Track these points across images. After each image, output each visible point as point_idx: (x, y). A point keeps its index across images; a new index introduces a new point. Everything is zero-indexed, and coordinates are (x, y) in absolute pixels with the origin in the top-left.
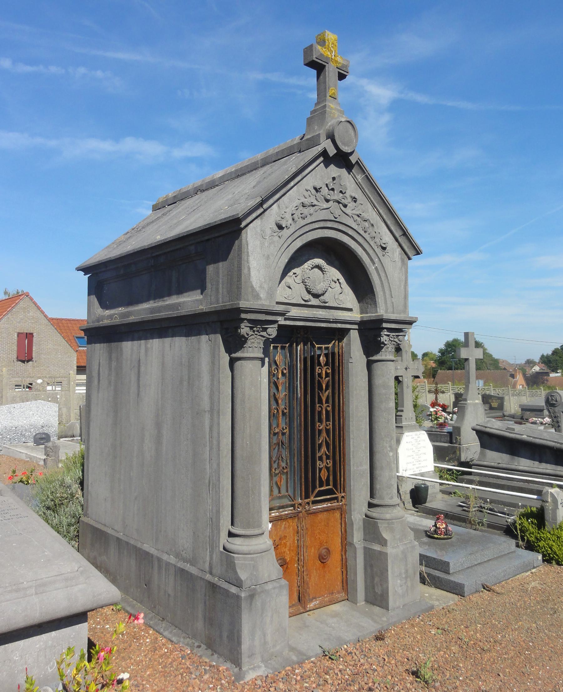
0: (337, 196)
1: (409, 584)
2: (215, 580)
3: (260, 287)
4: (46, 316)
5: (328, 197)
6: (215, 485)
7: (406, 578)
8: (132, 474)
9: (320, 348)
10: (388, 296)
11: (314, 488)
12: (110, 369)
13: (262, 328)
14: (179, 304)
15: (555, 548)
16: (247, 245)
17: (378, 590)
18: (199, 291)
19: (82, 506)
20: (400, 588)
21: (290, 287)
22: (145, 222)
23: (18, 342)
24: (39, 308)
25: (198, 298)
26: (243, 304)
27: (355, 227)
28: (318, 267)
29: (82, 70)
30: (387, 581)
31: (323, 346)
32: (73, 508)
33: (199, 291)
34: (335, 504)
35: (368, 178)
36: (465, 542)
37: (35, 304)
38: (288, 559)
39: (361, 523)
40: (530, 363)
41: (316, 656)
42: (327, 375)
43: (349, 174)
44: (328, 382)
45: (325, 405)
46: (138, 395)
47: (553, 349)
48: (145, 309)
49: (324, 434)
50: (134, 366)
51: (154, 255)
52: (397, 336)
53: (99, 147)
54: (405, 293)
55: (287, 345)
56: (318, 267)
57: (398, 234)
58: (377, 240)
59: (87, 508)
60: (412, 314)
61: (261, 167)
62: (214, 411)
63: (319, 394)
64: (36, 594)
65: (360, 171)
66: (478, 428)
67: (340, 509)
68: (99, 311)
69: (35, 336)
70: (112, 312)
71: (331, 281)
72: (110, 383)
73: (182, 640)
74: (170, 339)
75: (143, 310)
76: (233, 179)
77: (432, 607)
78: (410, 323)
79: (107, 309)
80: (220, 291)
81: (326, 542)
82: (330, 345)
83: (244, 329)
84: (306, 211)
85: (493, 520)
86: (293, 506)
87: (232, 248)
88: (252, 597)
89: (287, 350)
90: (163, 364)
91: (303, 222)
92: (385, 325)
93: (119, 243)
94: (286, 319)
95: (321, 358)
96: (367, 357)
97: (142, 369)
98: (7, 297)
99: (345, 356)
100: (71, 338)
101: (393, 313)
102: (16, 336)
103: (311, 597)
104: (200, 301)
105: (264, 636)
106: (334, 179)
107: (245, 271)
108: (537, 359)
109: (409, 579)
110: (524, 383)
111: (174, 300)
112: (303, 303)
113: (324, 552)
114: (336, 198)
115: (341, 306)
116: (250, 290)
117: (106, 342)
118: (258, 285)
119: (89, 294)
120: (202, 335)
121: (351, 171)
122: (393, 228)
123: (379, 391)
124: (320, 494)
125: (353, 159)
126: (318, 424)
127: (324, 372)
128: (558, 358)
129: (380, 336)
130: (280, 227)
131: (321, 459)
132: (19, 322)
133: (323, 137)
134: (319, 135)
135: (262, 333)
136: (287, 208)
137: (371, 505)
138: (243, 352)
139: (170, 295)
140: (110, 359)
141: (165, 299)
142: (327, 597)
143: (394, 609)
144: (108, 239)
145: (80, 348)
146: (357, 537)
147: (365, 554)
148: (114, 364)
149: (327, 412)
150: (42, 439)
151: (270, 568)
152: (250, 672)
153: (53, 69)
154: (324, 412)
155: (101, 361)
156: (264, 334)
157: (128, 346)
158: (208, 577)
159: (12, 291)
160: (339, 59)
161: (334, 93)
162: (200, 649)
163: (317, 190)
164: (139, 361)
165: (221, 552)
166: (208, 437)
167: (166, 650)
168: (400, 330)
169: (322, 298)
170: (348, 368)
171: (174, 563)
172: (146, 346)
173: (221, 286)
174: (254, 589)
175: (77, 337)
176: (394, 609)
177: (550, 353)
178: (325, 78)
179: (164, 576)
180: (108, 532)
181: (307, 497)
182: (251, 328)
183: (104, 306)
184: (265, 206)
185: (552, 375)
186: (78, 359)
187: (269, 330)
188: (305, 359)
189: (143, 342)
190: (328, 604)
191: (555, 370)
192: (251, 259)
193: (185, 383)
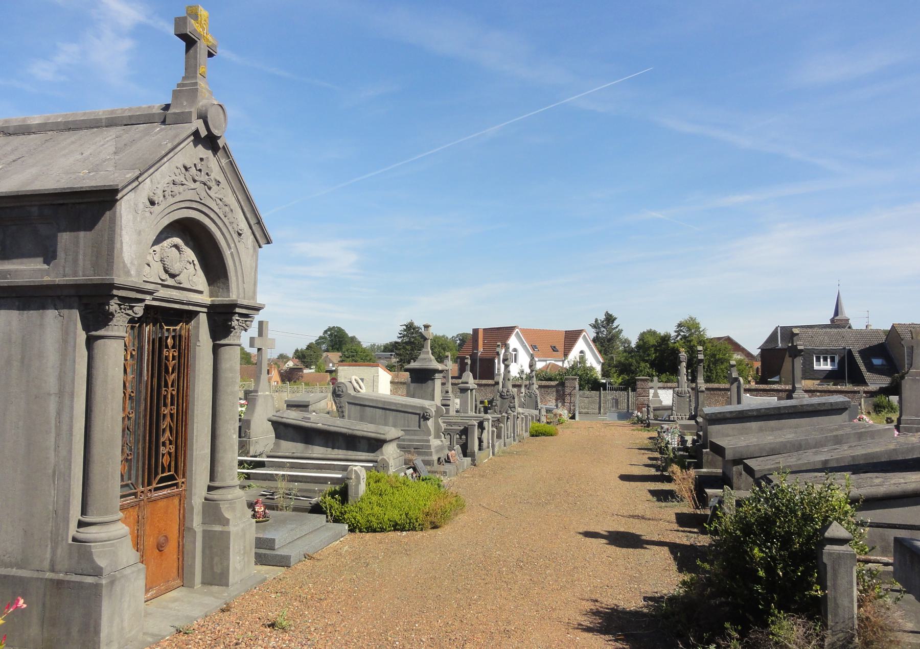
0: (204, 178)
1: (246, 559)
2: (61, 576)
3: (132, 263)
5: (197, 178)
6: (61, 475)
7: (244, 553)
9: (168, 330)
10: (240, 281)
11: (156, 474)
14: (9, 272)
15: (359, 518)
17: (217, 570)
18: (41, 259)
21: (149, 265)
26: (119, 280)
27: (217, 211)
28: (176, 246)
30: (228, 559)
31: (172, 328)
34: (175, 490)
35: (232, 164)
36: (283, 522)
39: (201, 508)
40: (283, 358)
41: (170, 634)
44: (175, 365)
45: (171, 389)
47: (308, 343)
49: (168, 419)
56: (176, 246)
57: (253, 221)
58: (235, 226)
60: (260, 300)
61: (107, 127)
62: (64, 393)
66: (274, 419)
67: (179, 495)
71: (186, 262)
76: (62, 130)
77: (265, 579)
80: (81, 262)
82: (178, 328)
83: (113, 306)
84: (176, 189)
85: (299, 504)
86: (135, 494)
87: (100, 219)
88: (112, 583)
89: (136, 331)
91: (173, 200)
92: (238, 310)
94: (154, 299)
95: (169, 340)
96: (213, 341)
99: (192, 340)
101: (244, 298)
105: (122, 621)
106: (202, 159)
107: (117, 245)
108: (291, 354)
110: (278, 379)
112: (160, 282)
113: (162, 539)
114: (202, 179)
116: (121, 265)
122: (248, 216)
123: (225, 375)
124: (162, 480)
125: (220, 143)
126: (163, 408)
128: (312, 353)
129: (231, 320)
130: (152, 203)
131: (164, 444)
133: (194, 116)
134: (190, 113)
135: (128, 312)
137: (210, 489)
138: (107, 330)
143: (233, 585)
146: (197, 522)
147: (204, 537)
151: (127, 554)
156: (130, 312)
158: (49, 575)
160: (209, 37)
163: (186, 169)
165: (70, 545)
166: (53, 422)
168: (246, 316)
169: (177, 278)
170: (195, 351)
173: (81, 257)
176: (233, 585)
177: (304, 347)
178: (196, 52)
181: (149, 484)
182: (119, 305)
184: (140, 179)
185: (306, 371)
187: (135, 309)
188: (153, 340)
191: (308, 366)
192: (124, 232)
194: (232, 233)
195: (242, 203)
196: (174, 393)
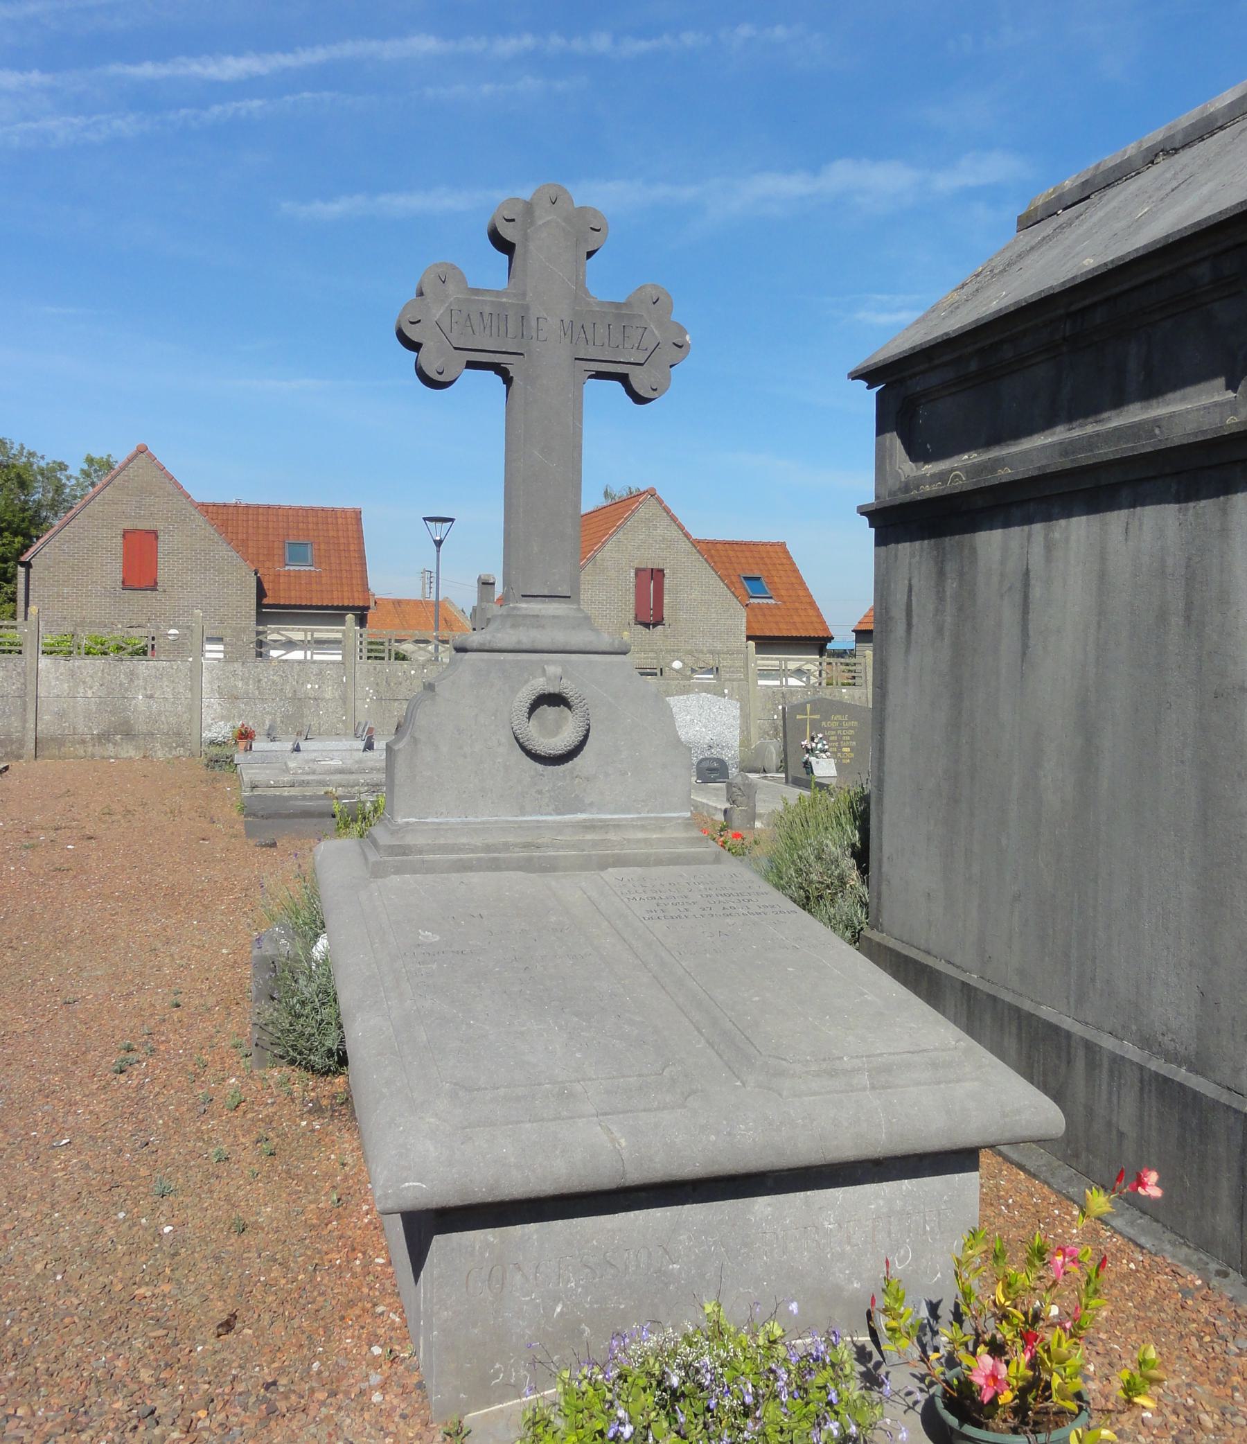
4: (687, 535)
8: (1004, 841)
12: (941, 598)
14: (1156, 422)
18: (1221, 381)
19: (865, 905)
22: (1008, 255)
23: (637, 586)
24: (674, 519)
25: (1217, 398)
29: (745, 31)
32: (846, 909)
33: (1221, 381)
37: (667, 511)
46: (1024, 654)
48: (1044, 447)
50: (1010, 588)
51: (1073, 308)
53: (780, 188)
59: (879, 911)
64: (873, 1088)
68: (906, 468)
69: (667, 576)
70: (943, 465)
72: (940, 631)
73: (1168, 1247)
74: (1124, 513)
75: (1036, 450)
79: (927, 461)
90: (1102, 575)
93: (955, 308)
97: (1036, 592)
98: (609, 502)
100: (734, 579)
102: (633, 574)
104: (1233, 407)
111: (1134, 414)
117: (930, 537)
119: (880, 431)
120: (1236, 492)
132: (638, 548)
139: (1119, 402)
140: (941, 574)
141: (1105, 415)
144: (901, 320)
145: (752, 601)
148: (951, 585)
150: (711, 770)
153: (689, 38)
155: (915, 581)
157: (993, 545)
159: (619, 491)
162: (1226, 1281)
164: (1027, 573)
167: (1132, 1266)
171: (1136, 1060)
172: (1046, 536)
175: (745, 578)
179: (1104, 1087)
180: (938, 968)
183: (917, 454)
186: (748, 622)
189: (1038, 527)
193: (1176, 621)
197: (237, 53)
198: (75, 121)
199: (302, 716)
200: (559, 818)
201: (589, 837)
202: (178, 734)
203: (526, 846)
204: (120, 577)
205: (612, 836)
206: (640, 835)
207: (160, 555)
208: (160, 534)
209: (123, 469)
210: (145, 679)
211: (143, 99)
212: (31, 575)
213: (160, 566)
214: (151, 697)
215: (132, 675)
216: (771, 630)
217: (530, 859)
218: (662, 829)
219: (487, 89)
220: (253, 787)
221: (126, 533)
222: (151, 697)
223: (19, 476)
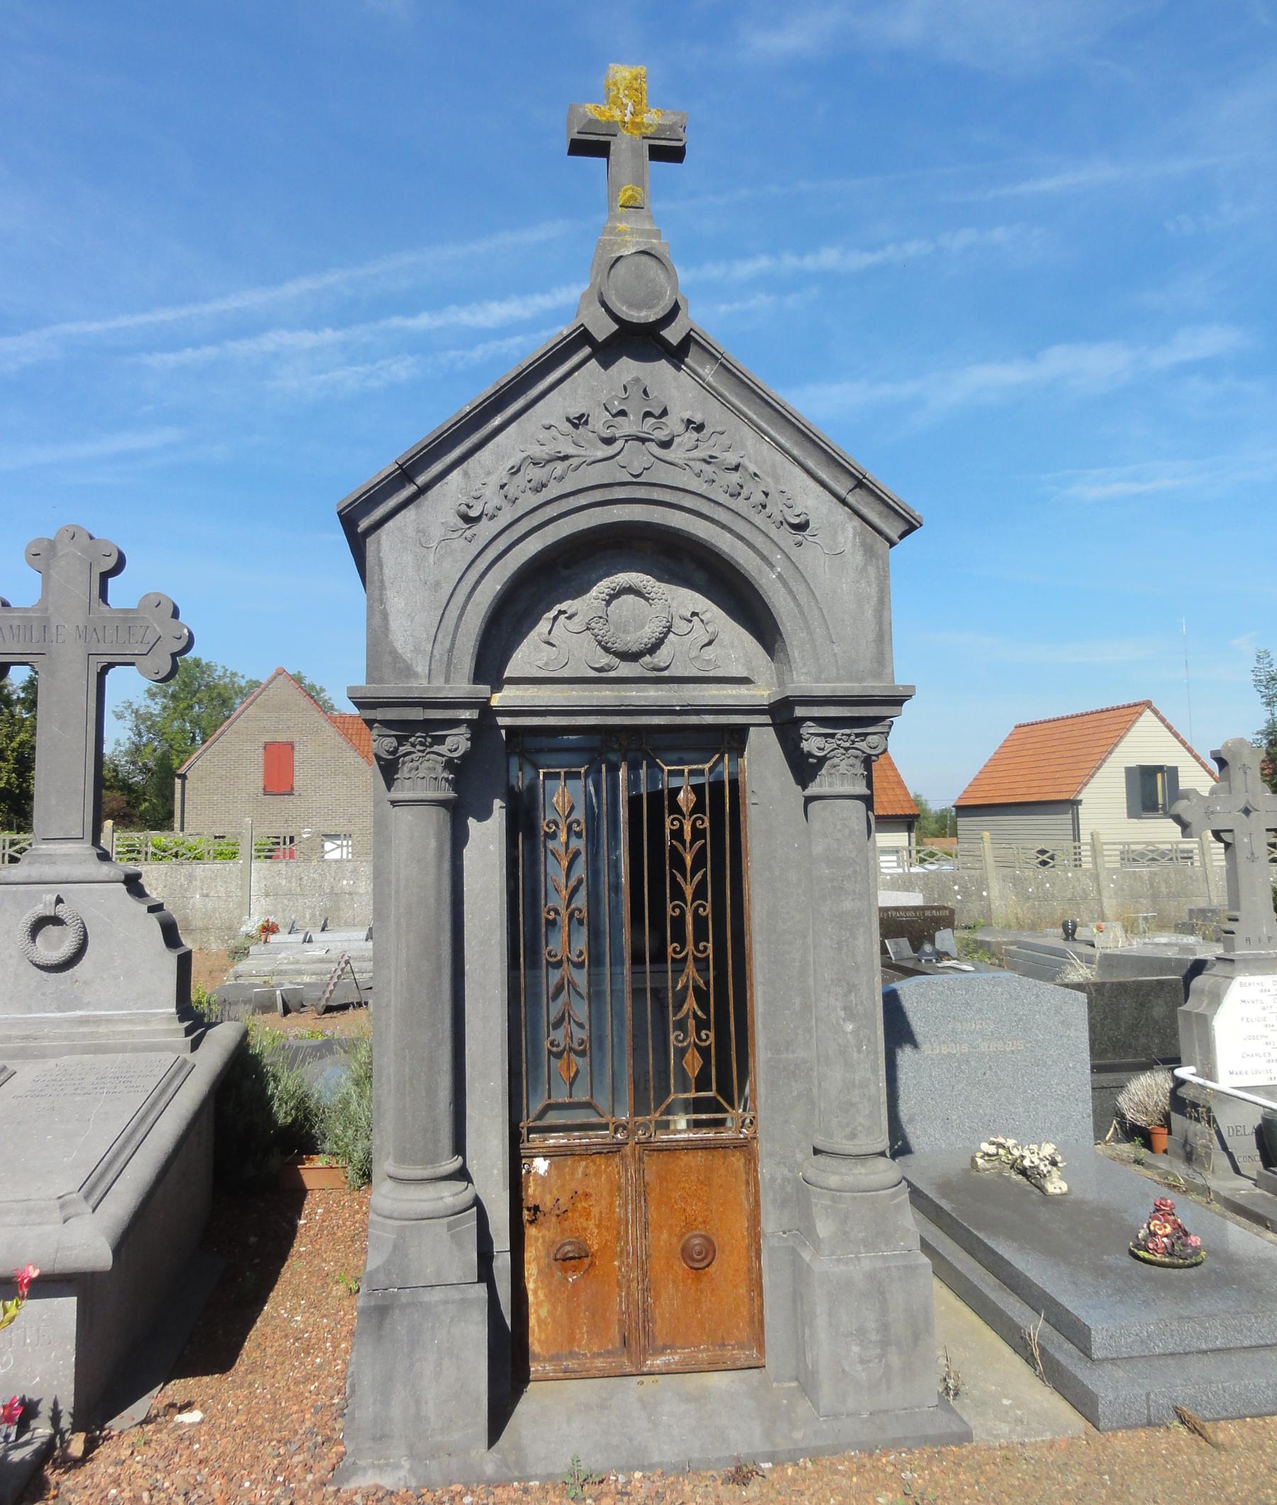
3: (417, 650)
13: (431, 737)
16: (381, 567)
20: (859, 1367)
27: (703, 488)
29: (966, 236)
35: (727, 369)
38: (596, 1247)
42: (697, 834)
43: (679, 369)
52: (857, 735)
53: (990, 378)
54: (881, 629)
55: (583, 770)
57: (842, 486)
60: (902, 677)
63: (673, 877)
65: (707, 356)
78: (898, 701)
81: (704, 1222)
103: (660, 1343)
105: (418, 1402)
109: (893, 1349)
114: (633, 430)
115: (711, 674)
118: (410, 647)
121: (683, 362)
127: (687, 828)
131: (681, 1025)
136: (488, 474)
142: (707, 1350)
149: (699, 922)
152: (370, 1472)
154: (689, 919)
161: (631, 197)
174: (394, 1295)
184: (421, 480)
190: (706, 1367)
194: (773, 532)
195: (795, 452)
196: (707, 911)
197: (501, 298)
198: (360, 369)
199: (339, 909)
200: (59, 1015)
201: (81, 1030)
202: (230, 928)
203: (26, 1038)
204: (261, 785)
205: (102, 1029)
206: (126, 1028)
207: (296, 764)
208: (296, 745)
209: (267, 686)
210: (202, 881)
211: (419, 345)
212: (187, 786)
213: (296, 773)
214: (207, 896)
215: (191, 878)
216: (893, 808)
217: (23, 1048)
218: (147, 1022)
219: (723, 308)
220: (236, 978)
221: (267, 746)
222: (207, 896)
223: (219, 694)
